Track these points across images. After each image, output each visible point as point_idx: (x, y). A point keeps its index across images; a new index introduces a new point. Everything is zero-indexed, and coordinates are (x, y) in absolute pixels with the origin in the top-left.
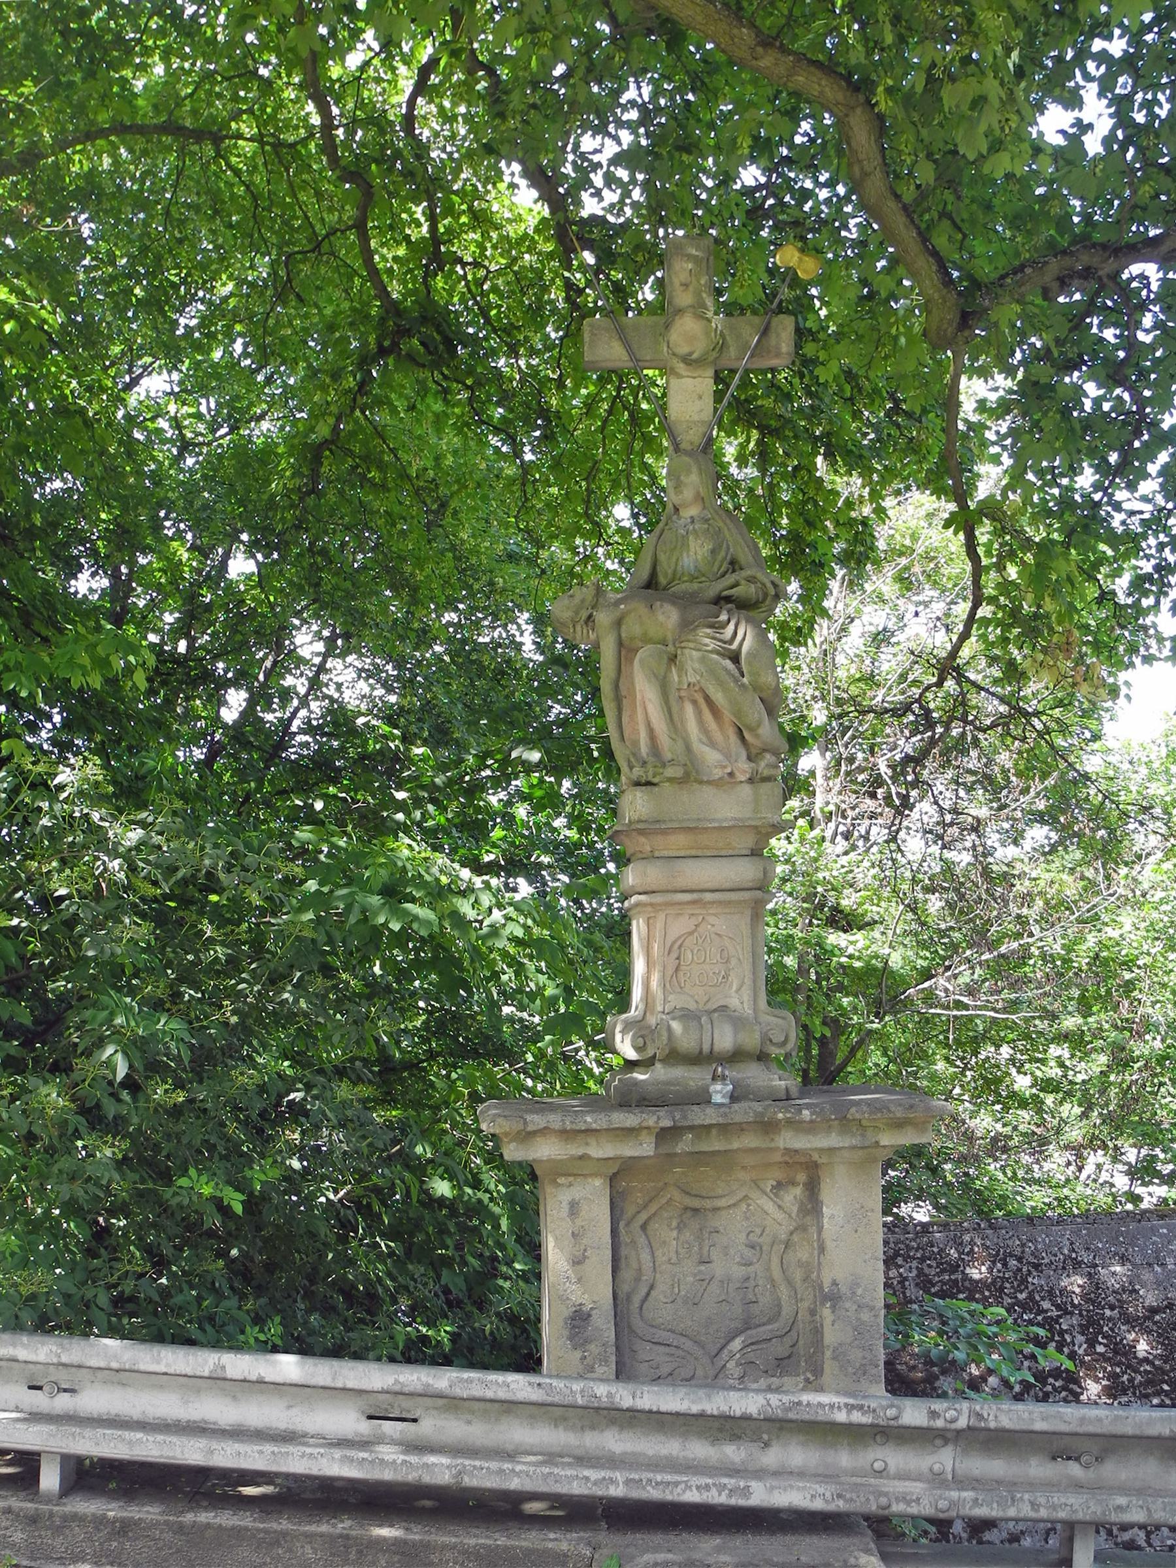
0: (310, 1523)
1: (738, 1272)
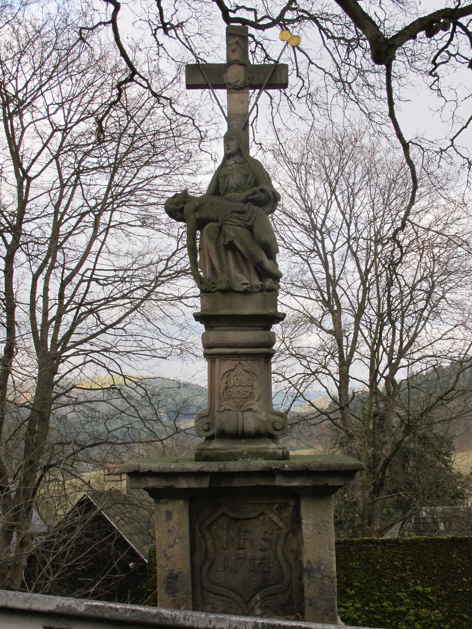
0: (290, 482)
1: (259, 554)
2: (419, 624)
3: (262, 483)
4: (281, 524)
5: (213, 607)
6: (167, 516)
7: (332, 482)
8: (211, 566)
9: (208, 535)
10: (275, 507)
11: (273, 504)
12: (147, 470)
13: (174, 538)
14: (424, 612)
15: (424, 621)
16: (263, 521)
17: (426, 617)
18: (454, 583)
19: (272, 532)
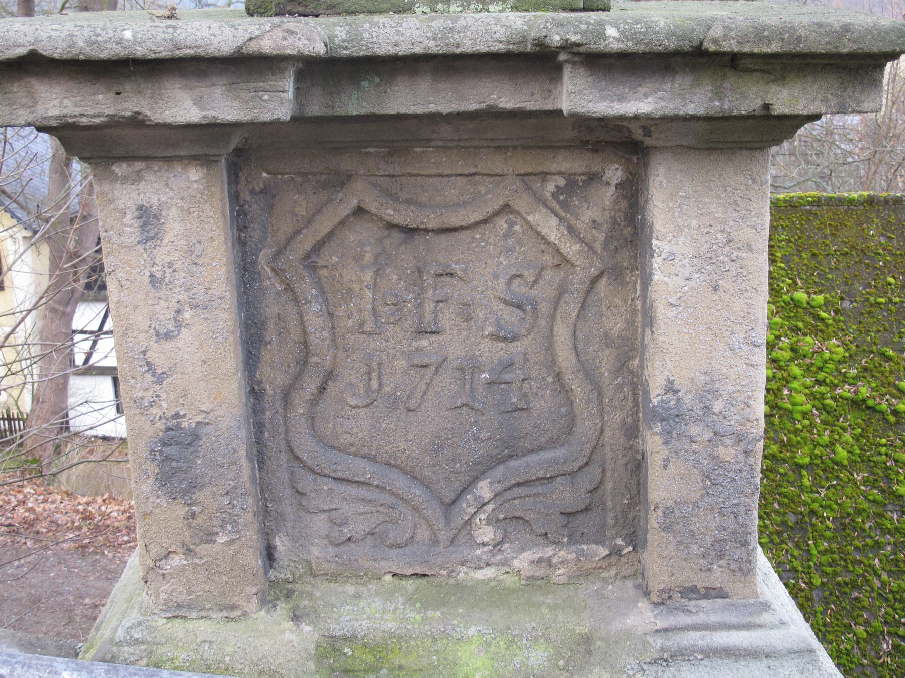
0: (621, 99)
1: (490, 352)
2: (799, 365)
3: (507, 102)
4: (570, 248)
5: (333, 522)
6: (144, 227)
7: (785, 99)
8: (322, 389)
9: (307, 288)
10: (550, 187)
11: (544, 176)
12: (22, 51)
13: (174, 305)
14: (809, 342)
15: (808, 361)
16: (506, 236)
17: (814, 353)
18: (869, 285)
19: (539, 276)
